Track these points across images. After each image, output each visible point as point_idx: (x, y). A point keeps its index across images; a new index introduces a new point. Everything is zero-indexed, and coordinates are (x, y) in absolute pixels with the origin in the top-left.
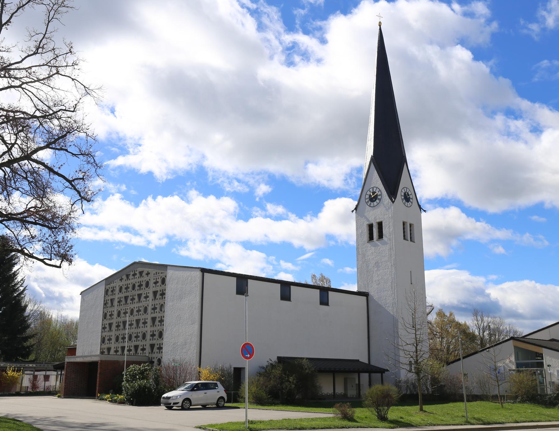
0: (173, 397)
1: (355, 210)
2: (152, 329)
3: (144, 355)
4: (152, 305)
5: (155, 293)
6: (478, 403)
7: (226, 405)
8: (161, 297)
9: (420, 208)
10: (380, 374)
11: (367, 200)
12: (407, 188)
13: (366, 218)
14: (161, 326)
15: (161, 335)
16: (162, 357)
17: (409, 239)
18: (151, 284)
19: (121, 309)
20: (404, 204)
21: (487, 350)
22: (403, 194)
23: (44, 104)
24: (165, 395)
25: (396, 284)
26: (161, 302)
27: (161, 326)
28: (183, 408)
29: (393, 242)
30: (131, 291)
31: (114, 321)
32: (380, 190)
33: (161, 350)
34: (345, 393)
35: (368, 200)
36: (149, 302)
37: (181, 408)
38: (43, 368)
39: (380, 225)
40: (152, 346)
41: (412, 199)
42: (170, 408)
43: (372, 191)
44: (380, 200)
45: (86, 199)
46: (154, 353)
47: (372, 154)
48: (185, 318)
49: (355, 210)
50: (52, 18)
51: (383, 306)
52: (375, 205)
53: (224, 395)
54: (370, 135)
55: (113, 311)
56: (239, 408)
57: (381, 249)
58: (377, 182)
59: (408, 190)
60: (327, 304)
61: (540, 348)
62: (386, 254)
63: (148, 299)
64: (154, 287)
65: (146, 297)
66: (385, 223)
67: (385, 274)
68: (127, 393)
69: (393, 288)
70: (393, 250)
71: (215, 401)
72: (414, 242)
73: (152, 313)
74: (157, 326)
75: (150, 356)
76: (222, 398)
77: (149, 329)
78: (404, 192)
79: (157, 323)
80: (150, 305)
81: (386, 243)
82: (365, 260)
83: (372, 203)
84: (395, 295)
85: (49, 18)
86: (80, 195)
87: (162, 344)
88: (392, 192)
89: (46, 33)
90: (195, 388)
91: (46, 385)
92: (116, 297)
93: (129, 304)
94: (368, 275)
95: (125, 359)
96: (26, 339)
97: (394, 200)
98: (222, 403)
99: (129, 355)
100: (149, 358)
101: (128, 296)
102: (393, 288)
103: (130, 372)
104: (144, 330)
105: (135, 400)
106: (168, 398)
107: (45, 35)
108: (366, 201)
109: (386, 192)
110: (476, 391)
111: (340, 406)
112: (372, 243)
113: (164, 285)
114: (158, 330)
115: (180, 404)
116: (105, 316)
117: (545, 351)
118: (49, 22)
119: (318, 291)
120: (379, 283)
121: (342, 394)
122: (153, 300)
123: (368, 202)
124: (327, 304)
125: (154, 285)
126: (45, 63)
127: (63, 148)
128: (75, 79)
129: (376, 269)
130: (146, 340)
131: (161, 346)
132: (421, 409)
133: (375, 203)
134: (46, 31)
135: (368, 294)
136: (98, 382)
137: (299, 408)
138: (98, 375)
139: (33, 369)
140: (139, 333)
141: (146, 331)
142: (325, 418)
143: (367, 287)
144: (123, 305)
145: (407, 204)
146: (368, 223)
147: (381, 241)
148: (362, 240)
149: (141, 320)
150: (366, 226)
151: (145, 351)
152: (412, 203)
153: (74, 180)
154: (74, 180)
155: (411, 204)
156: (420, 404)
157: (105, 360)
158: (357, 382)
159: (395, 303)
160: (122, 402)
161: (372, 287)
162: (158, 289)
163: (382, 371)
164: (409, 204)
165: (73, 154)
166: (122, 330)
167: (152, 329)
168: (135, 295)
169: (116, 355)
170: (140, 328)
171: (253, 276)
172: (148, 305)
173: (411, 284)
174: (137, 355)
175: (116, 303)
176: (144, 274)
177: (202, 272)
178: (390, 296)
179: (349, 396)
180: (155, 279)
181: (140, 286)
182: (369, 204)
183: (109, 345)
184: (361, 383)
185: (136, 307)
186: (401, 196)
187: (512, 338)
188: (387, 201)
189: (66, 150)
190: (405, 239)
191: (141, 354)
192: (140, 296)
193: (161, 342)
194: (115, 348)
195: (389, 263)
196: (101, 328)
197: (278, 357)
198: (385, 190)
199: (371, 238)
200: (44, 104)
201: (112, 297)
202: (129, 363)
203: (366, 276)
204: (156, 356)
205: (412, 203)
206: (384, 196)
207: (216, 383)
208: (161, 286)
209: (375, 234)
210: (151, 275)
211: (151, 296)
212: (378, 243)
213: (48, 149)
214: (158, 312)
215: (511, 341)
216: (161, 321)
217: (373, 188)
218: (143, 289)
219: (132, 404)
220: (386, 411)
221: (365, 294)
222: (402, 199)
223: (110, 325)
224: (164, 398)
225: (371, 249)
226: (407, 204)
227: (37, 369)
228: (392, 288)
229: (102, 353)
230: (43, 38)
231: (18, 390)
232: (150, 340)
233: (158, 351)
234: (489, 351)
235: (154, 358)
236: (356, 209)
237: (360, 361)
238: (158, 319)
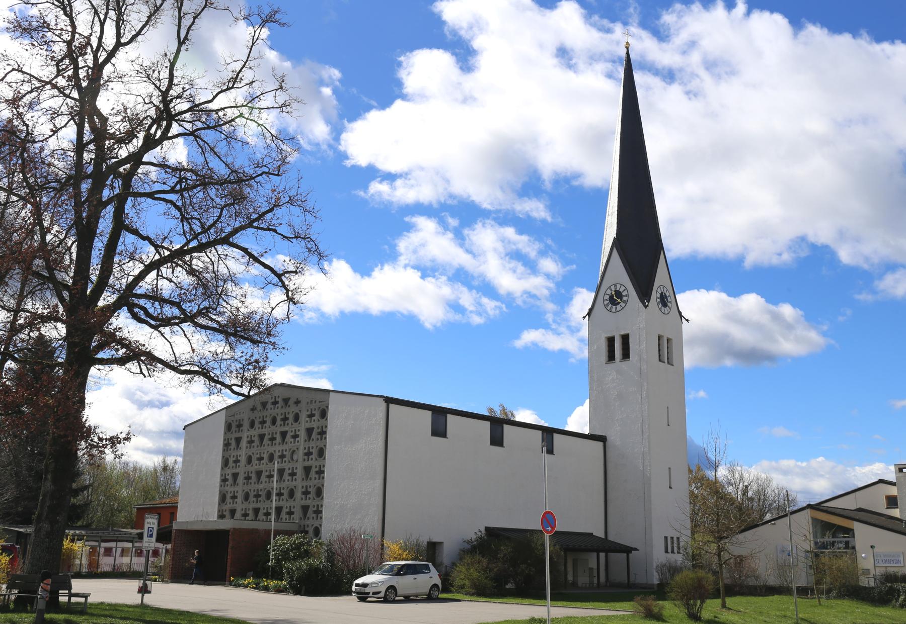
0: (372, 583)
2: (305, 484)
3: (291, 521)
4: (305, 448)
5: (309, 431)
6: (776, 598)
7: (442, 596)
8: (319, 437)
9: (681, 316)
10: (625, 554)
11: (606, 303)
14: (319, 479)
15: (319, 492)
16: (321, 525)
17: (666, 361)
18: (303, 417)
19: (253, 453)
20: (660, 309)
21: (773, 522)
22: (658, 295)
23: (221, 160)
24: (360, 581)
26: (229, 435)
27: (319, 479)
28: (386, 600)
30: (270, 427)
31: (242, 469)
32: (626, 289)
33: (319, 515)
34: (574, 579)
36: (299, 444)
37: (382, 599)
38: (97, 536)
39: (625, 339)
40: (305, 509)
41: (670, 302)
42: (363, 597)
44: (626, 302)
45: (292, 301)
46: (308, 518)
47: (615, 236)
48: (360, 469)
50: (257, 39)
53: (438, 581)
54: (611, 208)
55: (240, 456)
56: (459, 601)
58: (620, 276)
59: (665, 290)
61: (850, 521)
63: (297, 439)
64: (307, 421)
65: (295, 436)
68: (291, 577)
71: (427, 590)
72: (673, 365)
73: (304, 460)
74: (313, 479)
75: (303, 522)
76: (435, 586)
77: (299, 483)
79: (313, 474)
80: (302, 448)
83: (614, 307)
85: (253, 39)
86: (288, 296)
87: (322, 506)
88: (644, 294)
89: (247, 61)
90: (401, 571)
91: (116, 563)
92: (245, 435)
93: (266, 445)
95: (273, 528)
96: (76, 493)
97: (647, 304)
98: (436, 593)
99: (267, 521)
100: (300, 526)
101: (264, 435)
103: (280, 546)
104: (292, 484)
105: (304, 588)
106: (365, 585)
107: (245, 63)
110: (773, 582)
111: (641, 599)
112: (612, 365)
113: (325, 419)
114: (315, 486)
115: (382, 595)
116: (225, 463)
117: (857, 527)
118: (253, 44)
119: (540, 432)
122: (305, 441)
123: (607, 305)
125: (308, 419)
126: (245, 104)
127: (270, 227)
128: (262, 125)
130: (294, 500)
131: (320, 509)
132: (724, 606)
133: (618, 307)
134: (248, 57)
136: (229, 560)
137: (596, 604)
138: (229, 550)
139: (98, 539)
140: (283, 488)
141: (295, 487)
142: (609, 616)
144: (255, 447)
146: (606, 336)
149: (287, 469)
151: (292, 516)
152: (670, 308)
153: (283, 274)
154: (283, 274)
155: (669, 310)
156: (723, 596)
157: (240, 529)
160: (279, 590)
162: (314, 425)
163: (628, 550)
164: (666, 310)
165: (284, 237)
166: (255, 483)
167: (305, 484)
168: (276, 433)
169: (245, 520)
170: (284, 481)
171: (424, 404)
172: (298, 449)
174: (279, 521)
175: (244, 443)
176: (291, 402)
177: (386, 402)
179: (580, 584)
180: (310, 410)
181: (285, 419)
182: (609, 308)
183: (233, 506)
185: (277, 451)
186: (657, 297)
187: (809, 506)
189: (275, 231)
190: (660, 360)
191: (286, 519)
192: (284, 434)
193: (319, 503)
194: (242, 510)
196: (219, 480)
197: (486, 527)
199: (611, 357)
200: (221, 160)
201: (238, 435)
202: (277, 533)
204: (311, 523)
205: (670, 308)
207: (428, 565)
208: (319, 421)
209: (618, 353)
210: (303, 405)
211: (303, 434)
213: (250, 229)
214: (314, 459)
215: (809, 510)
216: (321, 472)
218: (290, 424)
219: (297, 592)
220: (699, 608)
221: (602, 439)
222: (658, 303)
223: (235, 476)
224: (357, 585)
227: (105, 538)
229: (221, 516)
230: (244, 66)
231: (76, 569)
232: (302, 499)
233: (315, 516)
234: (774, 524)
235: (308, 526)
236: (589, 314)
238: (314, 470)
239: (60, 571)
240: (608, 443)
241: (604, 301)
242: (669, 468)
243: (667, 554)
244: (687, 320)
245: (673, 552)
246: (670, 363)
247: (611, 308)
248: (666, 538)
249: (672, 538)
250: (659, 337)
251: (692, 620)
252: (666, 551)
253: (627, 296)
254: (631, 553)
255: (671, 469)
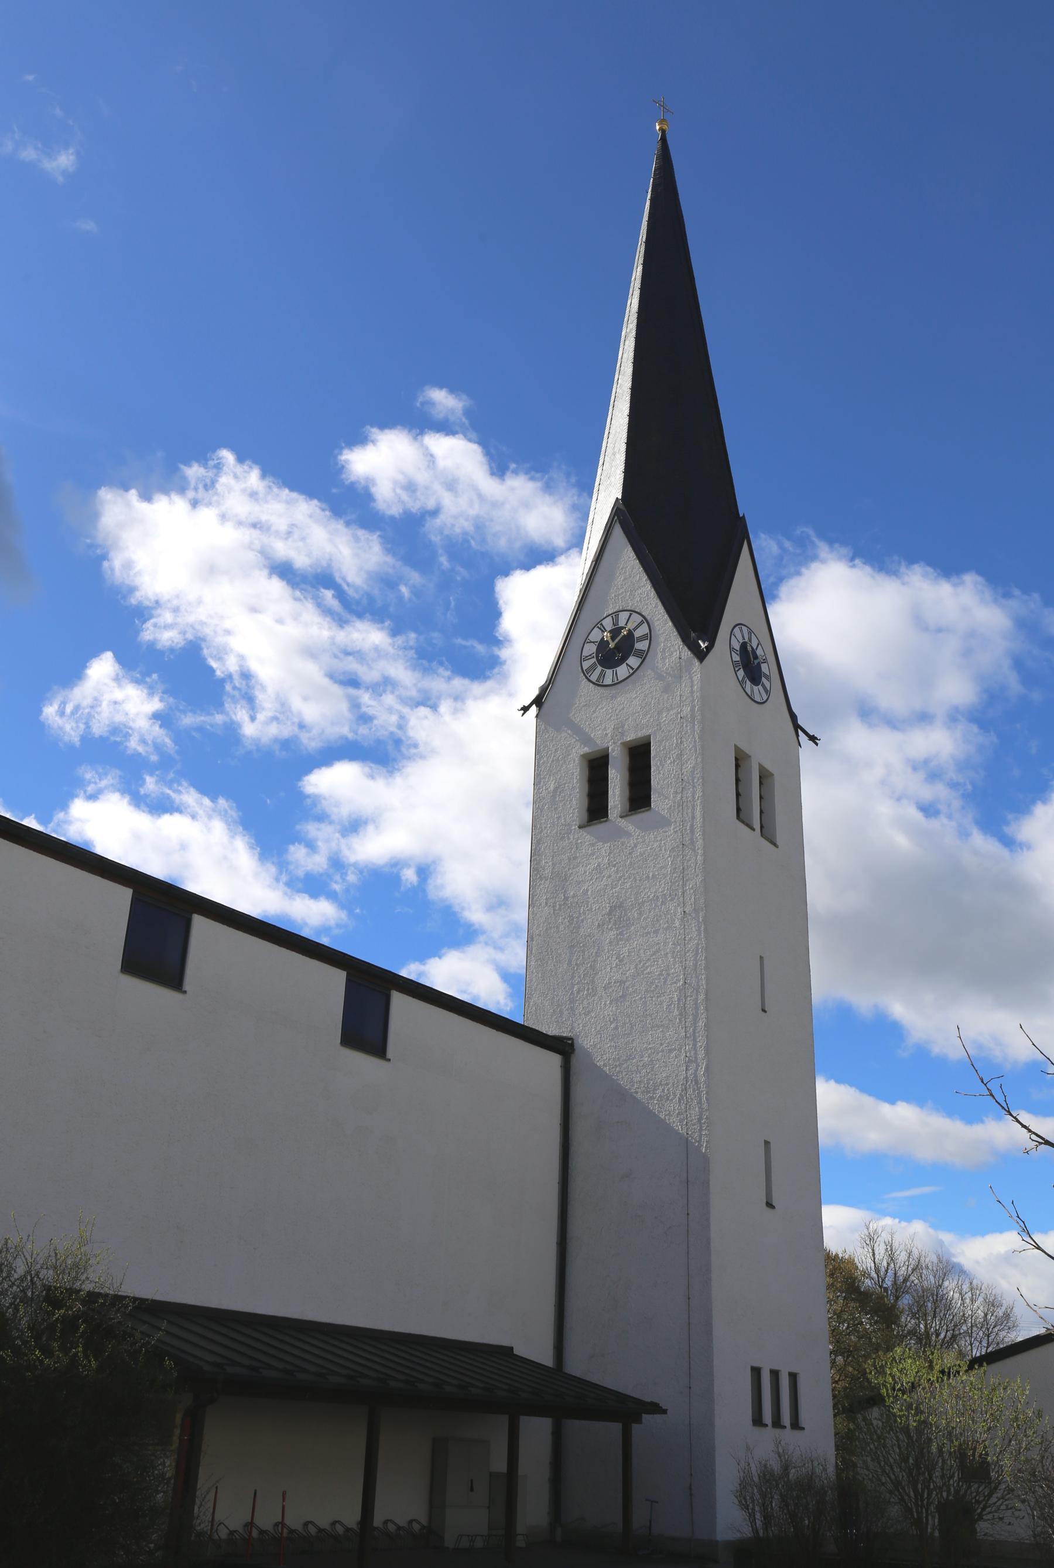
1: (534, 706)
9: (797, 727)
11: (586, 665)
12: (750, 632)
13: (576, 730)
17: (757, 825)
25: (702, 997)
29: (693, 817)
35: (594, 660)
43: (609, 628)
44: (643, 655)
49: (534, 706)
51: (639, 1096)
52: (620, 679)
57: (639, 850)
60: (377, 1047)
62: (662, 868)
66: (661, 742)
67: (654, 953)
69: (690, 1012)
70: (694, 850)
78: (741, 641)
81: (663, 822)
82: (566, 899)
84: (695, 1045)
94: (574, 963)
102: (690, 1012)
108: (585, 668)
109: (670, 623)
112: (599, 828)
120: (623, 996)
121: (416, 1527)
123: (592, 668)
124: (377, 1047)
129: (612, 934)
133: (622, 671)
135: (572, 1045)
143: (566, 1013)
145: (752, 691)
147: (642, 816)
148: (559, 818)
150: (577, 761)
158: (499, 1464)
159: (697, 1082)
161: (589, 1012)
164: (757, 691)
173: (764, 1011)
178: (670, 1051)
179: (449, 1541)
182: (594, 678)
184: (522, 1471)
186: (732, 649)
188: (676, 655)
195: (672, 906)
198: (666, 616)
203: (565, 966)
206: (662, 639)
209: (617, 792)
212: (628, 825)
217: (615, 615)
225: (593, 854)
226: (752, 691)
228: (683, 1014)
236: (538, 701)
237: (515, 1352)
239: (991, 1472)
240: (576, 1061)
241: (582, 659)
242: (767, 1143)
243: (778, 1431)
244: (813, 739)
245: (777, 1423)
246: (767, 833)
247: (602, 675)
248: (756, 1372)
249: (775, 1374)
250: (737, 759)
251: (159, 816)
252: (758, 1421)
253: (649, 637)
254: (638, 1420)
255: (773, 1146)
